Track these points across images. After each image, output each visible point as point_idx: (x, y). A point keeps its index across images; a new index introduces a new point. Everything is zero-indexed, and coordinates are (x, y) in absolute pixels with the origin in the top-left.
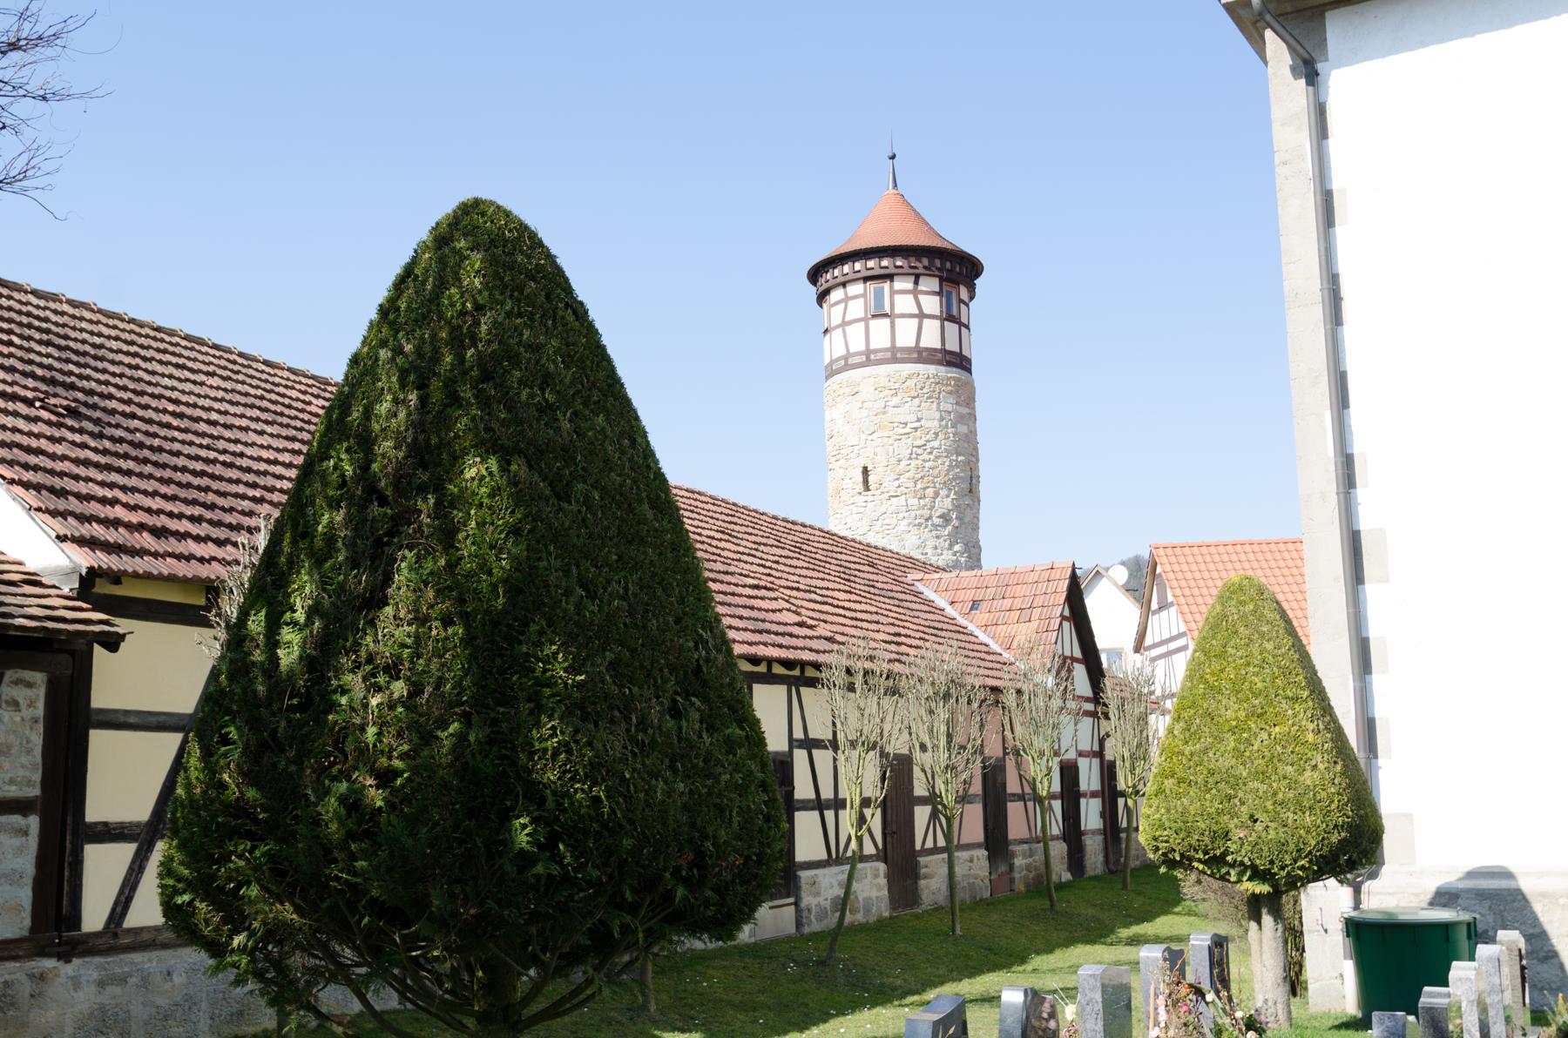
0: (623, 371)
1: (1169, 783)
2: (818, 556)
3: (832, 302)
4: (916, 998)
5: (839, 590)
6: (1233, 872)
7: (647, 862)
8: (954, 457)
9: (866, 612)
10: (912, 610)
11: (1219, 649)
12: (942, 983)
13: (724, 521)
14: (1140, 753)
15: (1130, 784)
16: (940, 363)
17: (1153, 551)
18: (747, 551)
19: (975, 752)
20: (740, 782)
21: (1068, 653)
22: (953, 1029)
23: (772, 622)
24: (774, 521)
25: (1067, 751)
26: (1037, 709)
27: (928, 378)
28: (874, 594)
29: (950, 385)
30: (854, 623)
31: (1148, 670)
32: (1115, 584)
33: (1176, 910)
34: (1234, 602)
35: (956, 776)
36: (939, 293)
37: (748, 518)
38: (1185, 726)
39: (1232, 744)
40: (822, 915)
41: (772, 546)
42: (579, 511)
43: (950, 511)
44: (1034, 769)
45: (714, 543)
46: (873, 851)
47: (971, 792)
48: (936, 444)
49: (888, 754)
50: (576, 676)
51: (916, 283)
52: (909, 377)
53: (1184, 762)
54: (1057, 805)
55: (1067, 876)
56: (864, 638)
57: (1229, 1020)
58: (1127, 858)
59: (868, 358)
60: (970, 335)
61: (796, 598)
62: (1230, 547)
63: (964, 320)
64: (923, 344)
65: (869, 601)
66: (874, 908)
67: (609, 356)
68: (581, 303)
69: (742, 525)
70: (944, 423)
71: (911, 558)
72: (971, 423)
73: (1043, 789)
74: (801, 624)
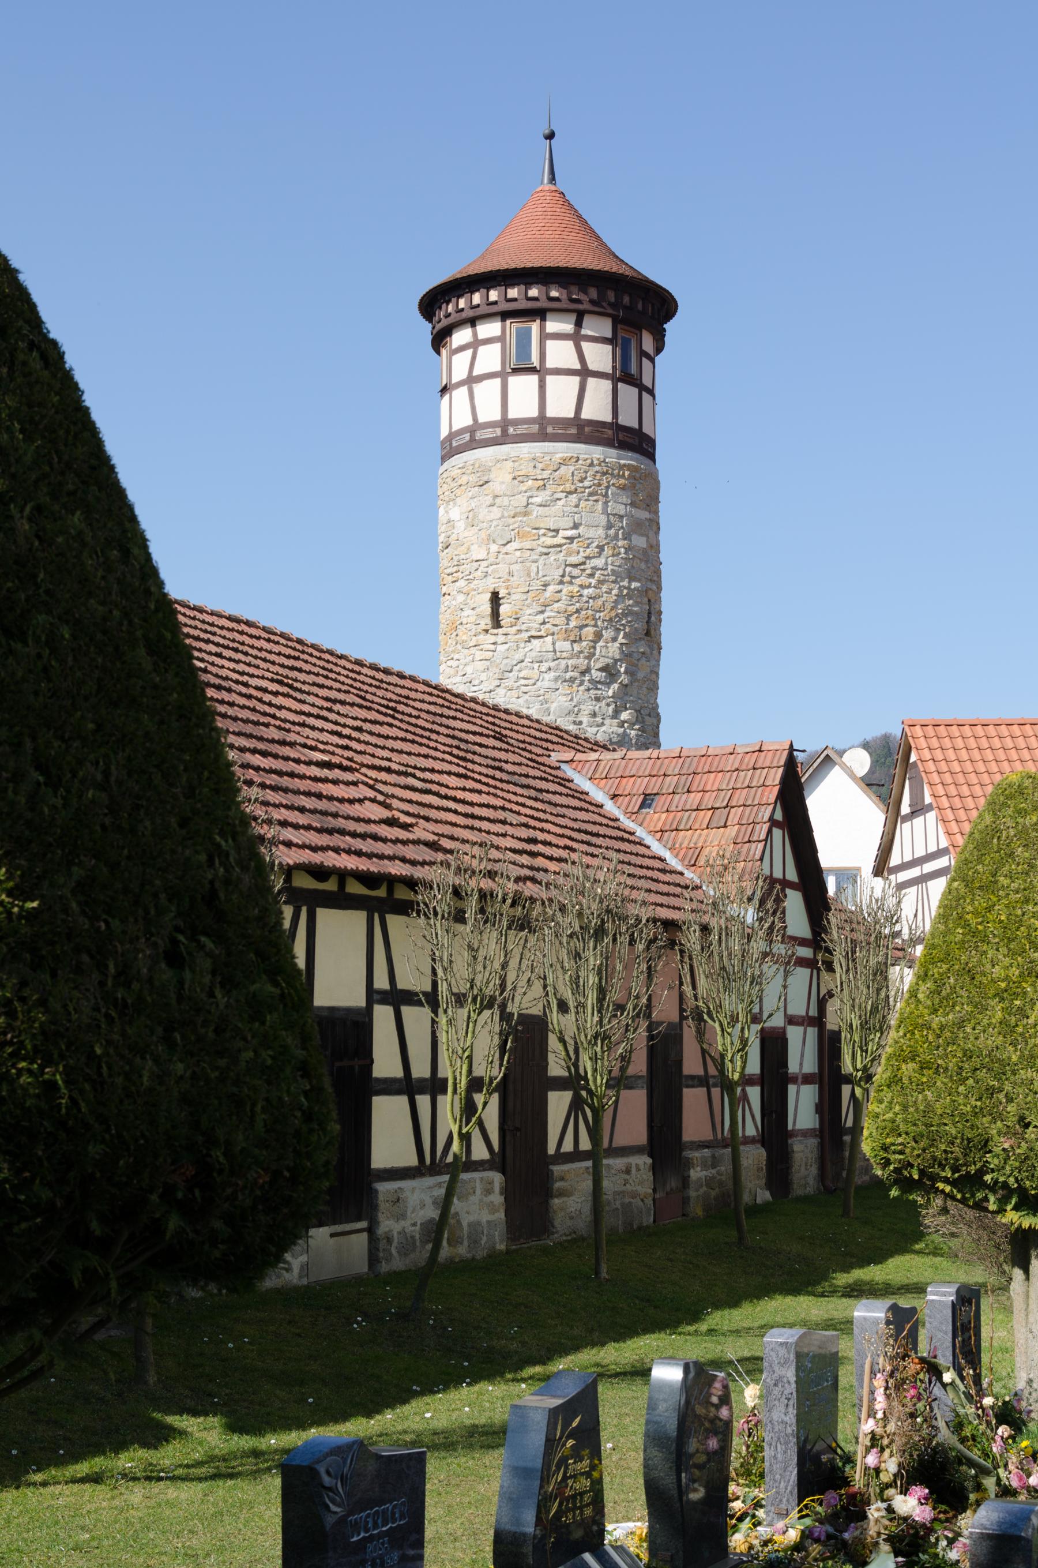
0: (112, 447)
1: (908, 1069)
2: (420, 722)
3: (454, 346)
4: (538, 1369)
5: (449, 773)
6: (992, 1199)
7: (124, 1179)
8: (625, 583)
9: (488, 806)
10: (556, 805)
11: (986, 878)
12: (576, 1349)
13: (282, 666)
14: (875, 1022)
15: (859, 1066)
16: (608, 443)
17: (907, 729)
18: (315, 711)
19: (638, 1015)
20: (269, 1062)
21: (778, 874)
22: (578, 1420)
23: (348, 818)
24: (357, 668)
25: (771, 1015)
26: (730, 954)
27: (592, 465)
28: (501, 781)
29: (623, 476)
30: (470, 822)
31: (891, 902)
32: (851, 775)
33: (917, 1247)
34: (1010, 811)
35: (609, 1049)
36: (611, 341)
37: (318, 662)
38: (933, 988)
39: (999, 1015)
40: (408, 1245)
41: (352, 705)
42: (39, 656)
43: (616, 661)
44: (723, 1042)
45: (267, 698)
46: (485, 1155)
47: (631, 1071)
48: (599, 562)
49: (511, 1014)
50: (25, 901)
51: (579, 324)
52: (564, 462)
53: (930, 1038)
54: (754, 1093)
55: (764, 1196)
56: (481, 845)
57: (973, 1410)
58: (850, 1172)
59: (505, 432)
60: (654, 404)
61: (385, 783)
62: (1015, 727)
63: (647, 381)
64: (585, 415)
65: (492, 790)
66: (485, 1238)
67: (93, 423)
68: (54, 343)
69: (309, 673)
70: (612, 532)
71: (557, 728)
72: (651, 534)
73: (734, 1071)
74: (391, 822)
